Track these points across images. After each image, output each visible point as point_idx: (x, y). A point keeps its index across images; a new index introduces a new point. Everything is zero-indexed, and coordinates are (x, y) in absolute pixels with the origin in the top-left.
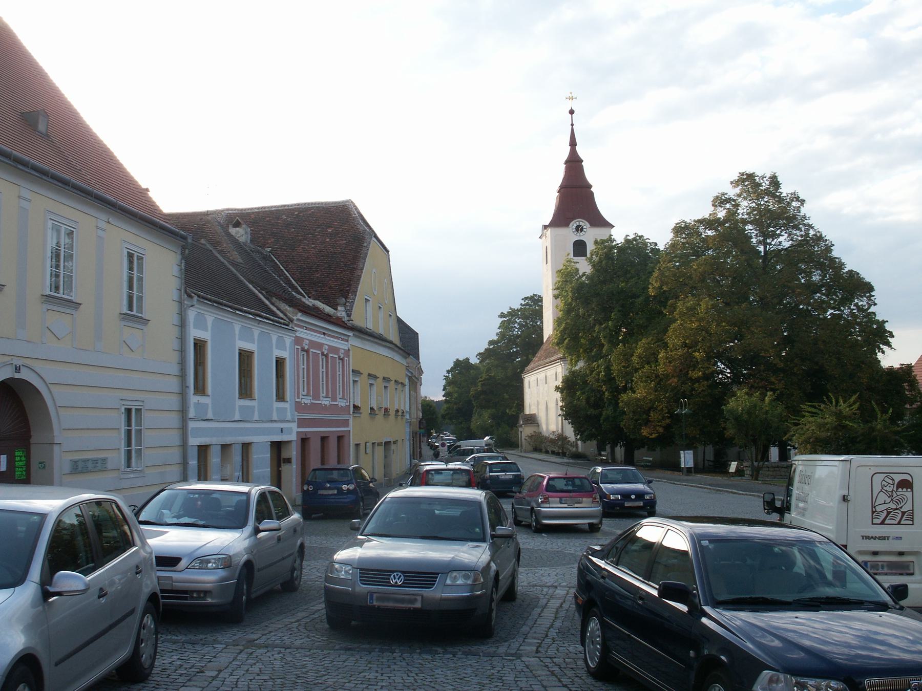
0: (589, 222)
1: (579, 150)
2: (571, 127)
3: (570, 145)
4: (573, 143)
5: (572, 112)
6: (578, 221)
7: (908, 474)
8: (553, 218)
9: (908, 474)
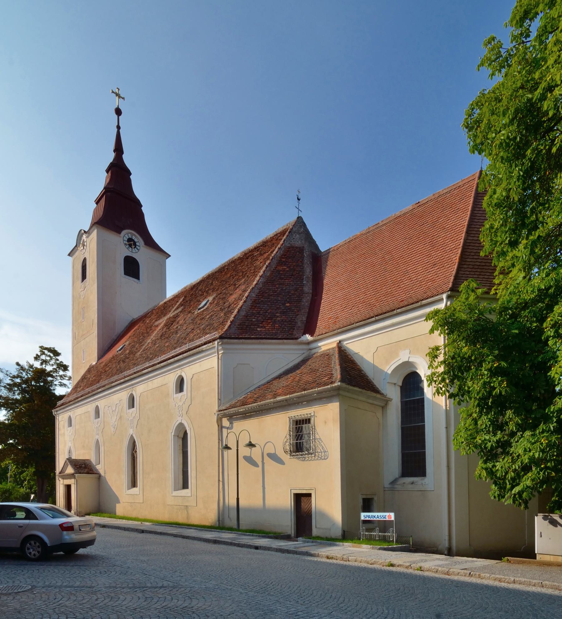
0: (141, 236)
1: (127, 159)
2: (116, 130)
3: (114, 151)
4: (119, 149)
5: (118, 112)
6: (131, 233)
7: (266, 444)
8: (114, 160)
9: (266, 444)
